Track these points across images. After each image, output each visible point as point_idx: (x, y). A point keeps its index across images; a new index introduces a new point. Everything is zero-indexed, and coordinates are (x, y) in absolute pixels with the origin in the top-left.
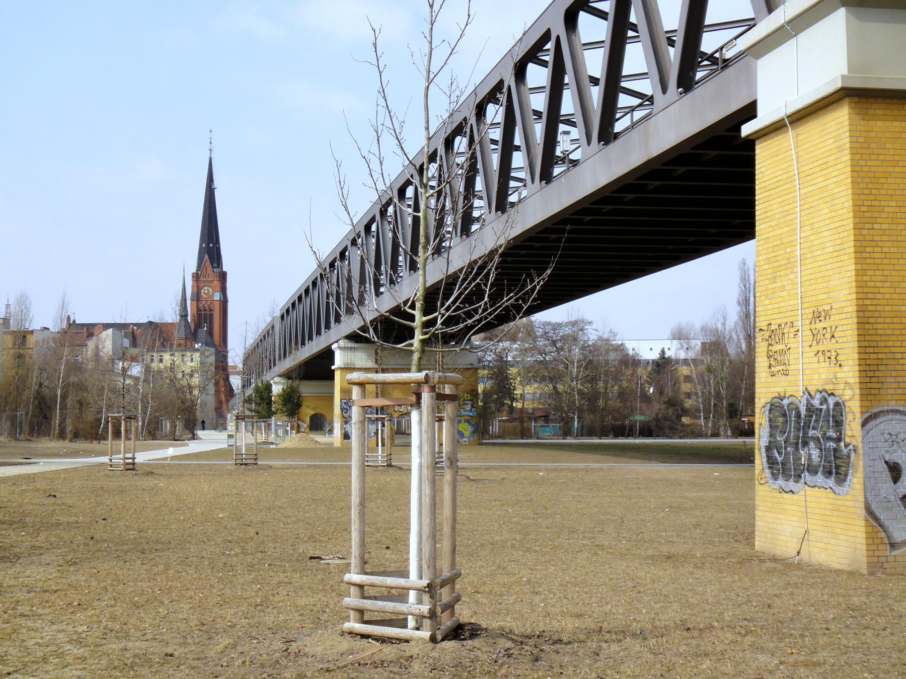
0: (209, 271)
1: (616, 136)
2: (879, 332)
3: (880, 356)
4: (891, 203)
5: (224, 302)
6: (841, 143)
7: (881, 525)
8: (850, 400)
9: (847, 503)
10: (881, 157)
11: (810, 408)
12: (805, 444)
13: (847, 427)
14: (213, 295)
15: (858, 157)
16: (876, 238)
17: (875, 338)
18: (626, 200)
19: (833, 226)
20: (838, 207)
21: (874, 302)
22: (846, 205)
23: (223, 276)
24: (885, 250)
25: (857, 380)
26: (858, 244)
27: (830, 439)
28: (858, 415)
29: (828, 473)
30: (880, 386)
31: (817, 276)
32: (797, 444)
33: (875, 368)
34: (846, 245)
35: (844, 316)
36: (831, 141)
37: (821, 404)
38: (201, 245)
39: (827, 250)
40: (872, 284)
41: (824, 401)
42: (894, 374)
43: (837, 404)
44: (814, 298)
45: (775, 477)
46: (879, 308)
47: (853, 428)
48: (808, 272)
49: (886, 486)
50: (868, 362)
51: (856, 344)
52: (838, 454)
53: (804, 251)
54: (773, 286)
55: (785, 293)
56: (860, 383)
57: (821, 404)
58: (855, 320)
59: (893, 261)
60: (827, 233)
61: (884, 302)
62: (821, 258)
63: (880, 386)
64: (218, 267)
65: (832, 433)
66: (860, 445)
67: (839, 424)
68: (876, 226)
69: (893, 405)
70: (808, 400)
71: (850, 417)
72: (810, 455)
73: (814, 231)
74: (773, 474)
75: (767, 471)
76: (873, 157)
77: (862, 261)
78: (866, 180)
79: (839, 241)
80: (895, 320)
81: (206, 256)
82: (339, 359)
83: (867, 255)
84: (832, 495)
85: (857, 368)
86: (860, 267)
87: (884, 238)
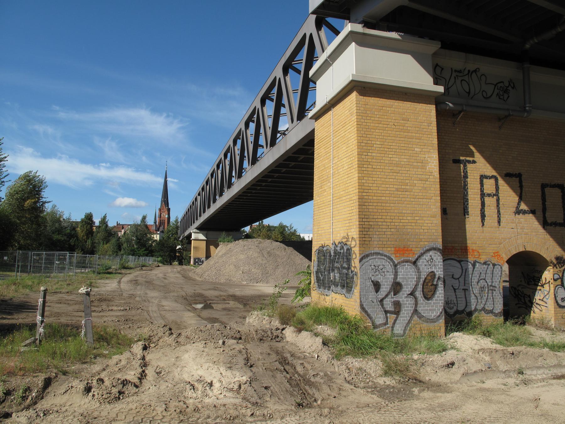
2: (370, 210)
3: (371, 223)
4: (377, 143)
6: (352, 111)
7: (368, 315)
8: (354, 247)
9: (352, 303)
10: (372, 119)
11: (335, 252)
12: (333, 270)
13: (353, 262)
15: (361, 117)
16: (369, 160)
17: (368, 213)
19: (348, 155)
20: (350, 145)
21: (368, 194)
22: (354, 142)
23: (169, 210)
24: (374, 167)
25: (358, 236)
26: (360, 163)
27: (344, 268)
28: (358, 255)
29: (343, 287)
30: (370, 239)
31: (340, 182)
32: (329, 270)
33: (368, 230)
34: (354, 164)
35: (352, 202)
36: (348, 111)
37: (341, 250)
39: (345, 168)
40: (367, 185)
41: (342, 248)
42: (377, 233)
43: (348, 249)
44: (338, 194)
45: (319, 287)
46: (370, 197)
47: (356, 263)
48: (336, 181)
49: (372, 295)
50: (364, 226)
51: (358, 216)
52: (348, 276)
53: (334, 170)
54: (321, 190)
55: (326, 193)
56: (360, 238)
57: (341, 250)
58: (357, 203)
59: (378, 173)
60: (345, 159)
61: (373, 194)
62: (342, 173)
63: (370, 239)
65: (345, 265)
66: (359, 272)
67: (349, 261)
68: (369, 154)
69: (376, 250)
70: (334, 247)
71: (354, 256)
72: (335, 276)
73: (339, 159)
74: (318, 285)
75: (316, 283)
76: (368, 118)
77: (362, 172)
78: (364, 130)
79: (351, 163)
80: (378, 204)
82: (193, 236)
83: (365, 169)
84: (345, 298)
85: (358, 230)
86: (360, 175)
87: (373, 161)
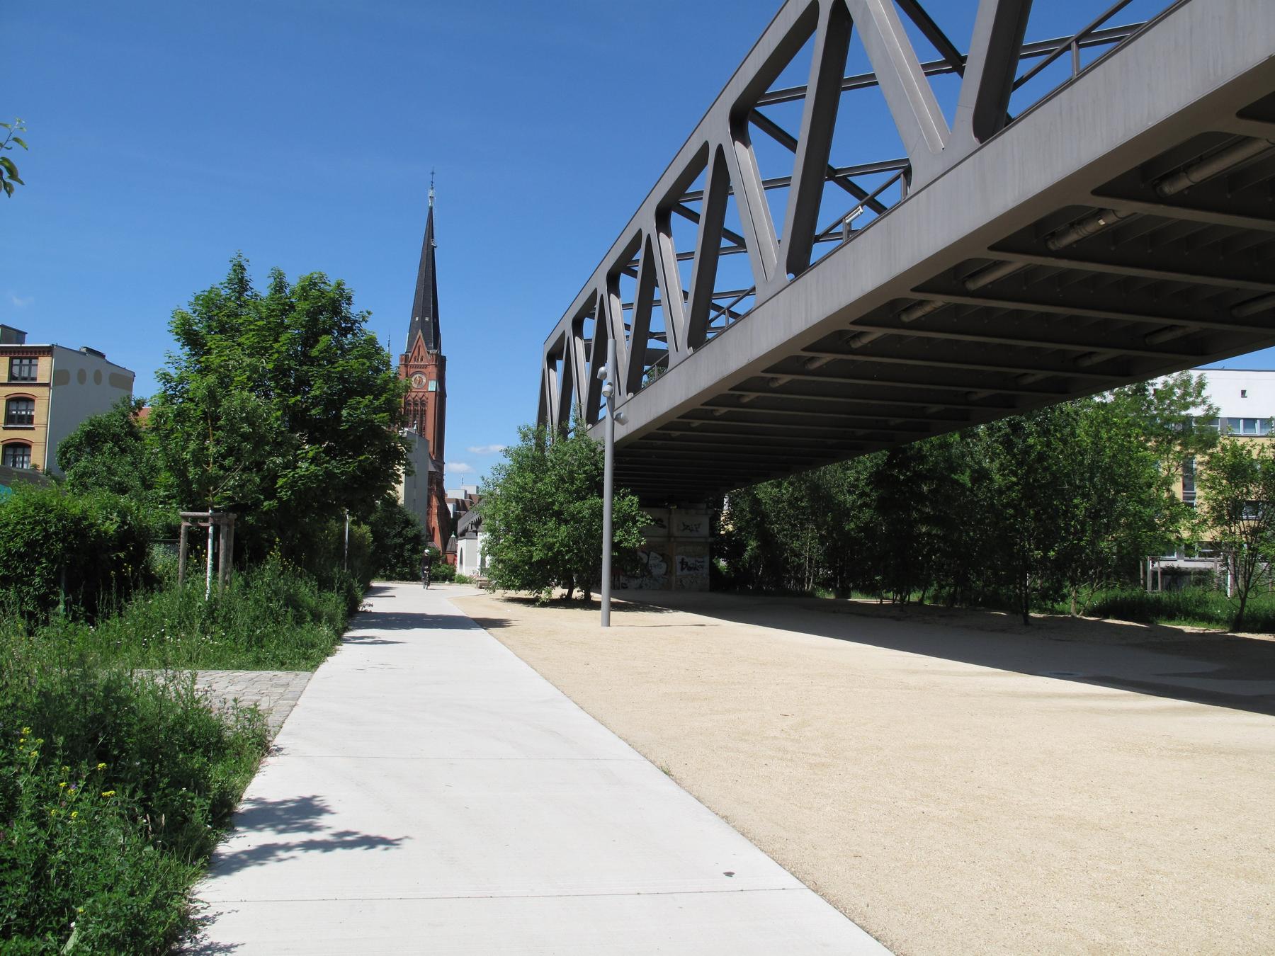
0: (422, 353)
1: (1009, 122)
5: (441, 395)
14: (427, 384)
18: (717, 414)
23: (441, 362)
38: (413, 318)
64: (435, 347)
81: (420, 333)
